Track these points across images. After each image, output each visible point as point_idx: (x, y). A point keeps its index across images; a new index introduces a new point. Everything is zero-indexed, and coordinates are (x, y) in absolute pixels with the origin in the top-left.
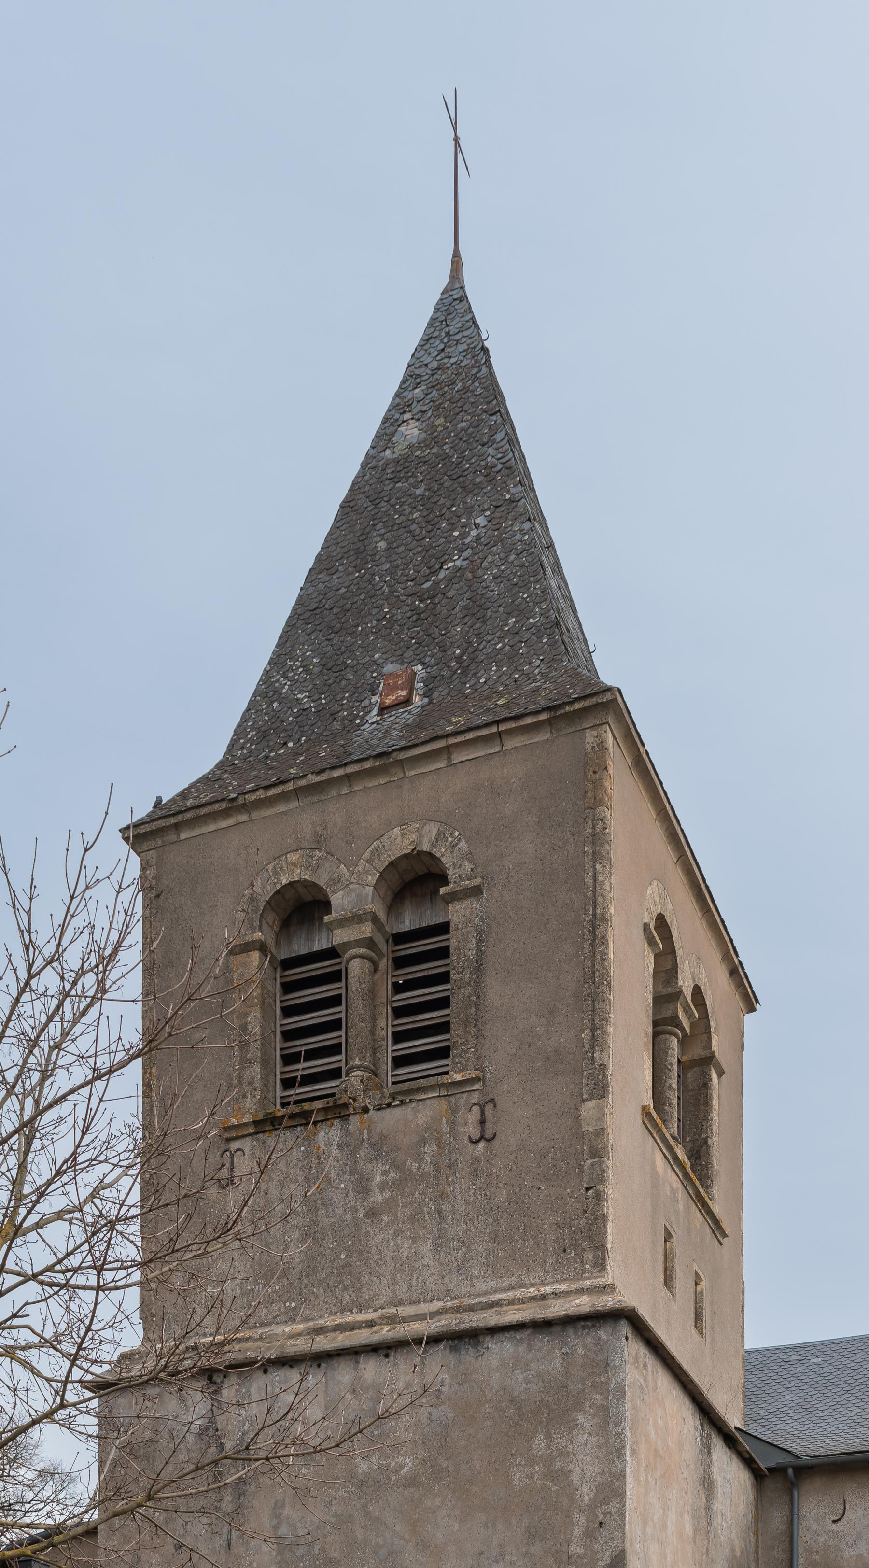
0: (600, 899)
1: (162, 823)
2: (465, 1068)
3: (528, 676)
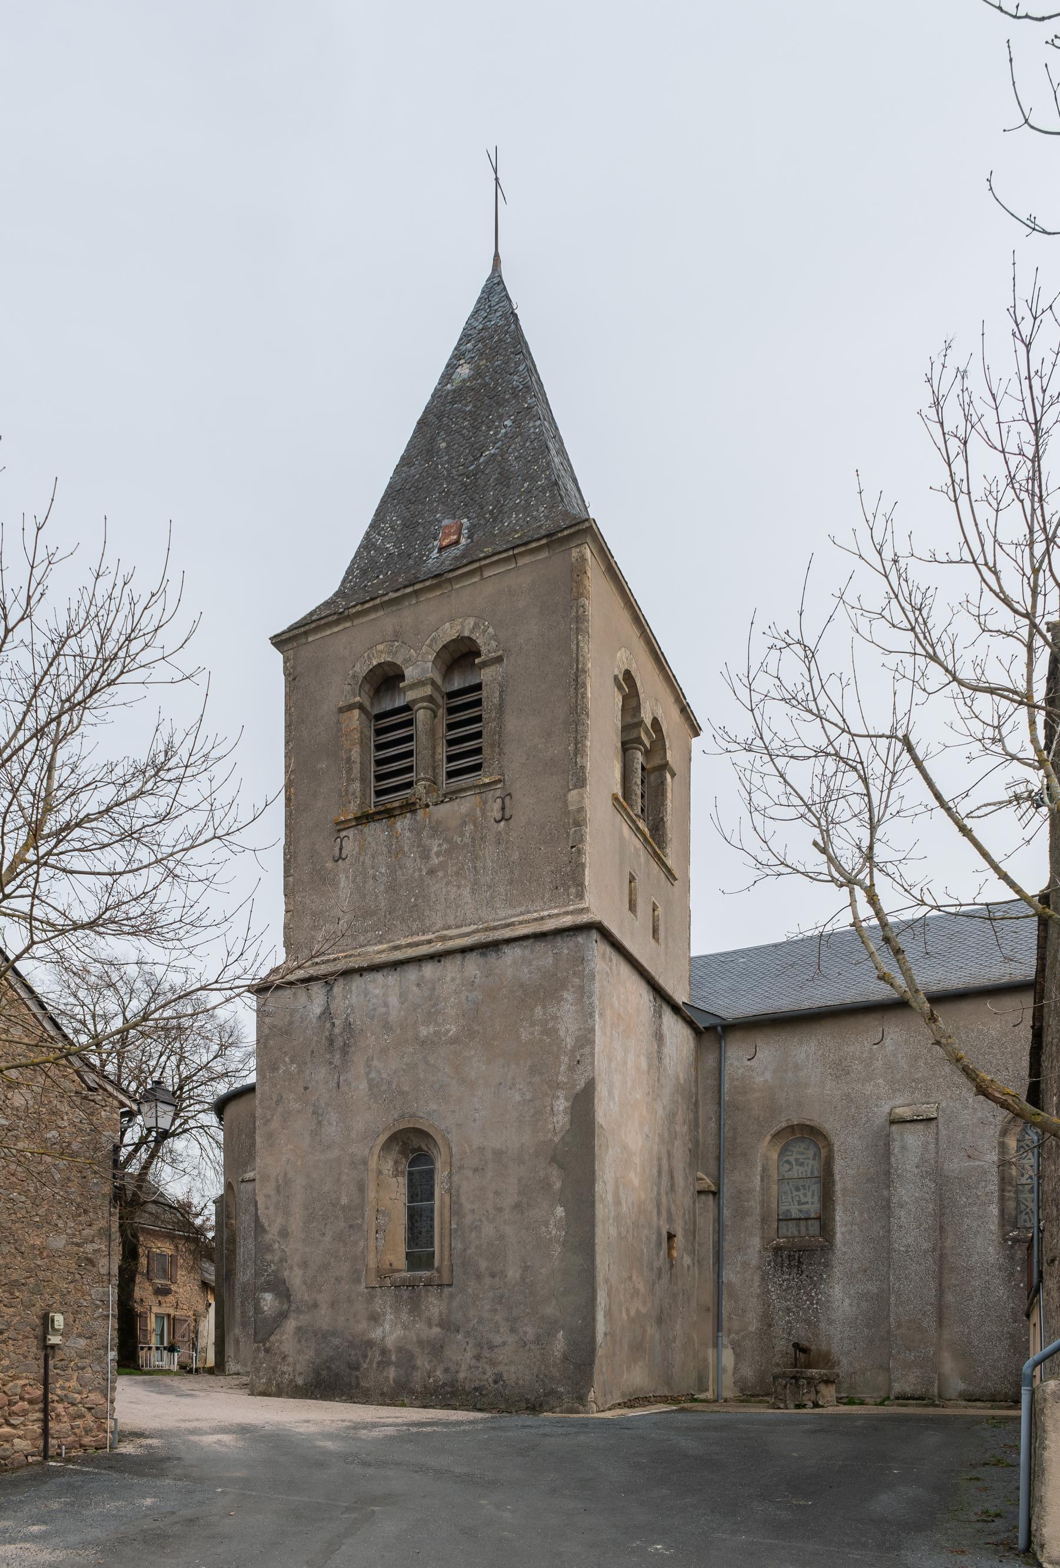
0: (581, 658)
1: (296, 632)
2: (491, 775)
3: (535, 518)
